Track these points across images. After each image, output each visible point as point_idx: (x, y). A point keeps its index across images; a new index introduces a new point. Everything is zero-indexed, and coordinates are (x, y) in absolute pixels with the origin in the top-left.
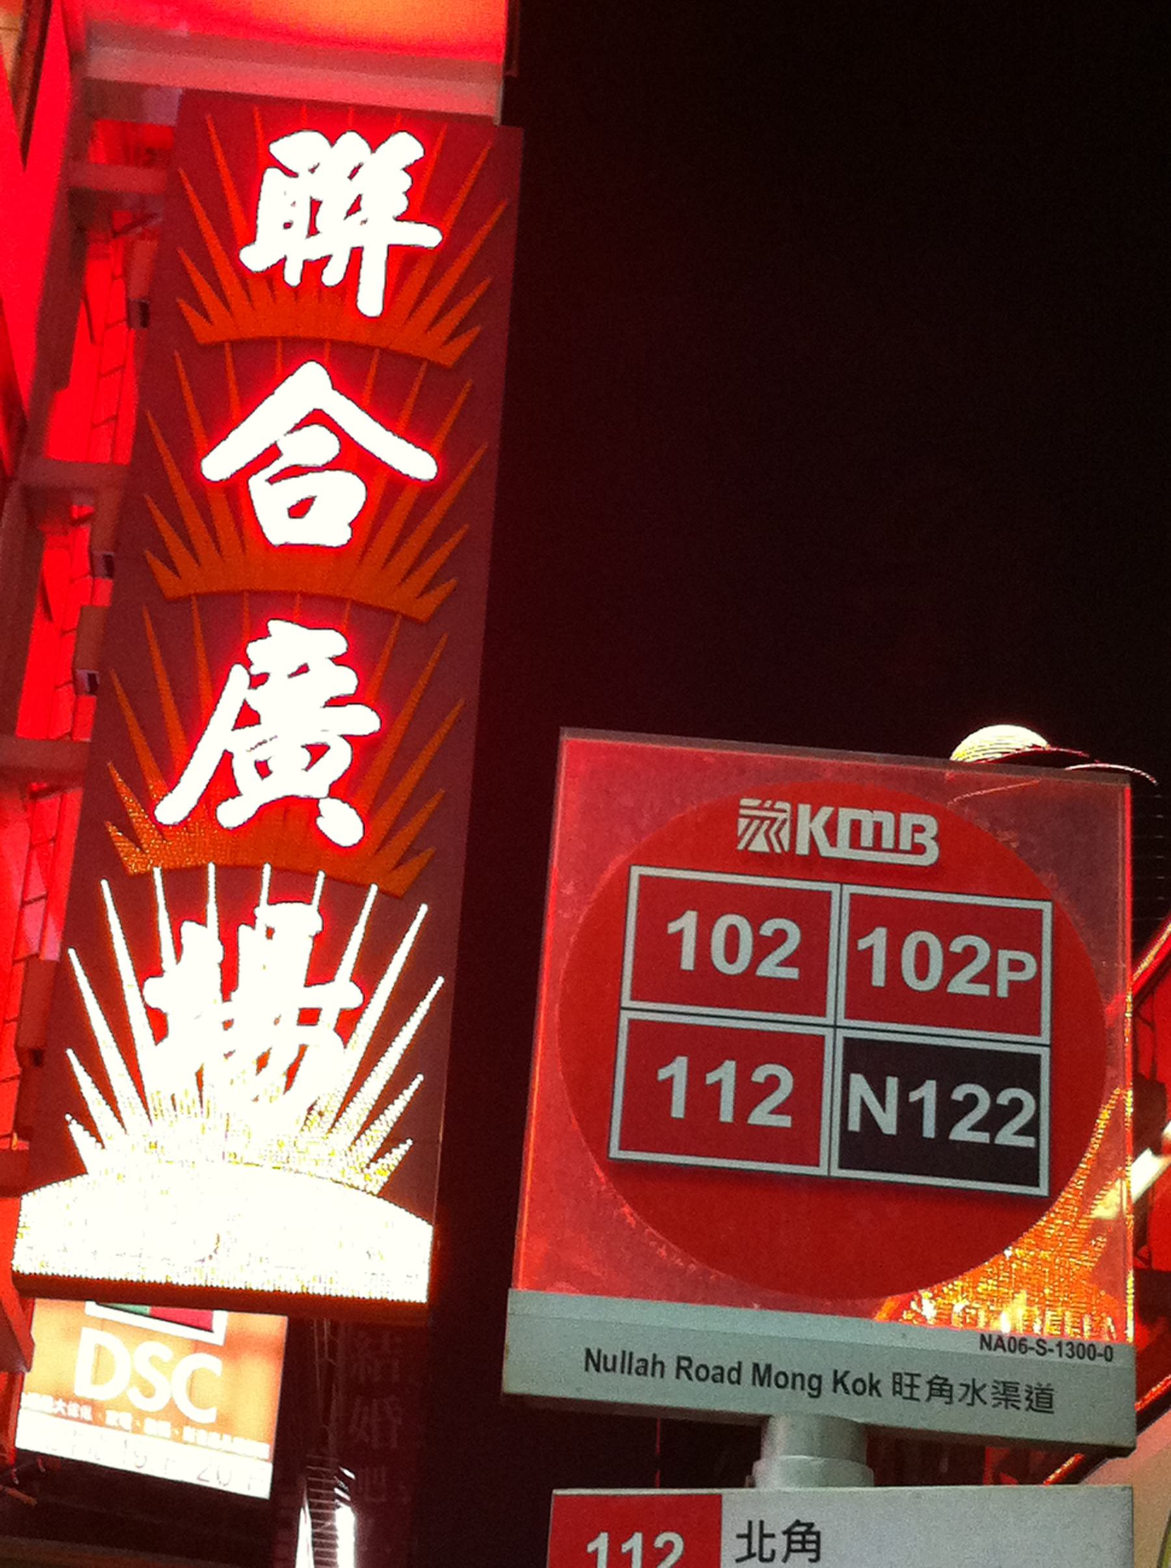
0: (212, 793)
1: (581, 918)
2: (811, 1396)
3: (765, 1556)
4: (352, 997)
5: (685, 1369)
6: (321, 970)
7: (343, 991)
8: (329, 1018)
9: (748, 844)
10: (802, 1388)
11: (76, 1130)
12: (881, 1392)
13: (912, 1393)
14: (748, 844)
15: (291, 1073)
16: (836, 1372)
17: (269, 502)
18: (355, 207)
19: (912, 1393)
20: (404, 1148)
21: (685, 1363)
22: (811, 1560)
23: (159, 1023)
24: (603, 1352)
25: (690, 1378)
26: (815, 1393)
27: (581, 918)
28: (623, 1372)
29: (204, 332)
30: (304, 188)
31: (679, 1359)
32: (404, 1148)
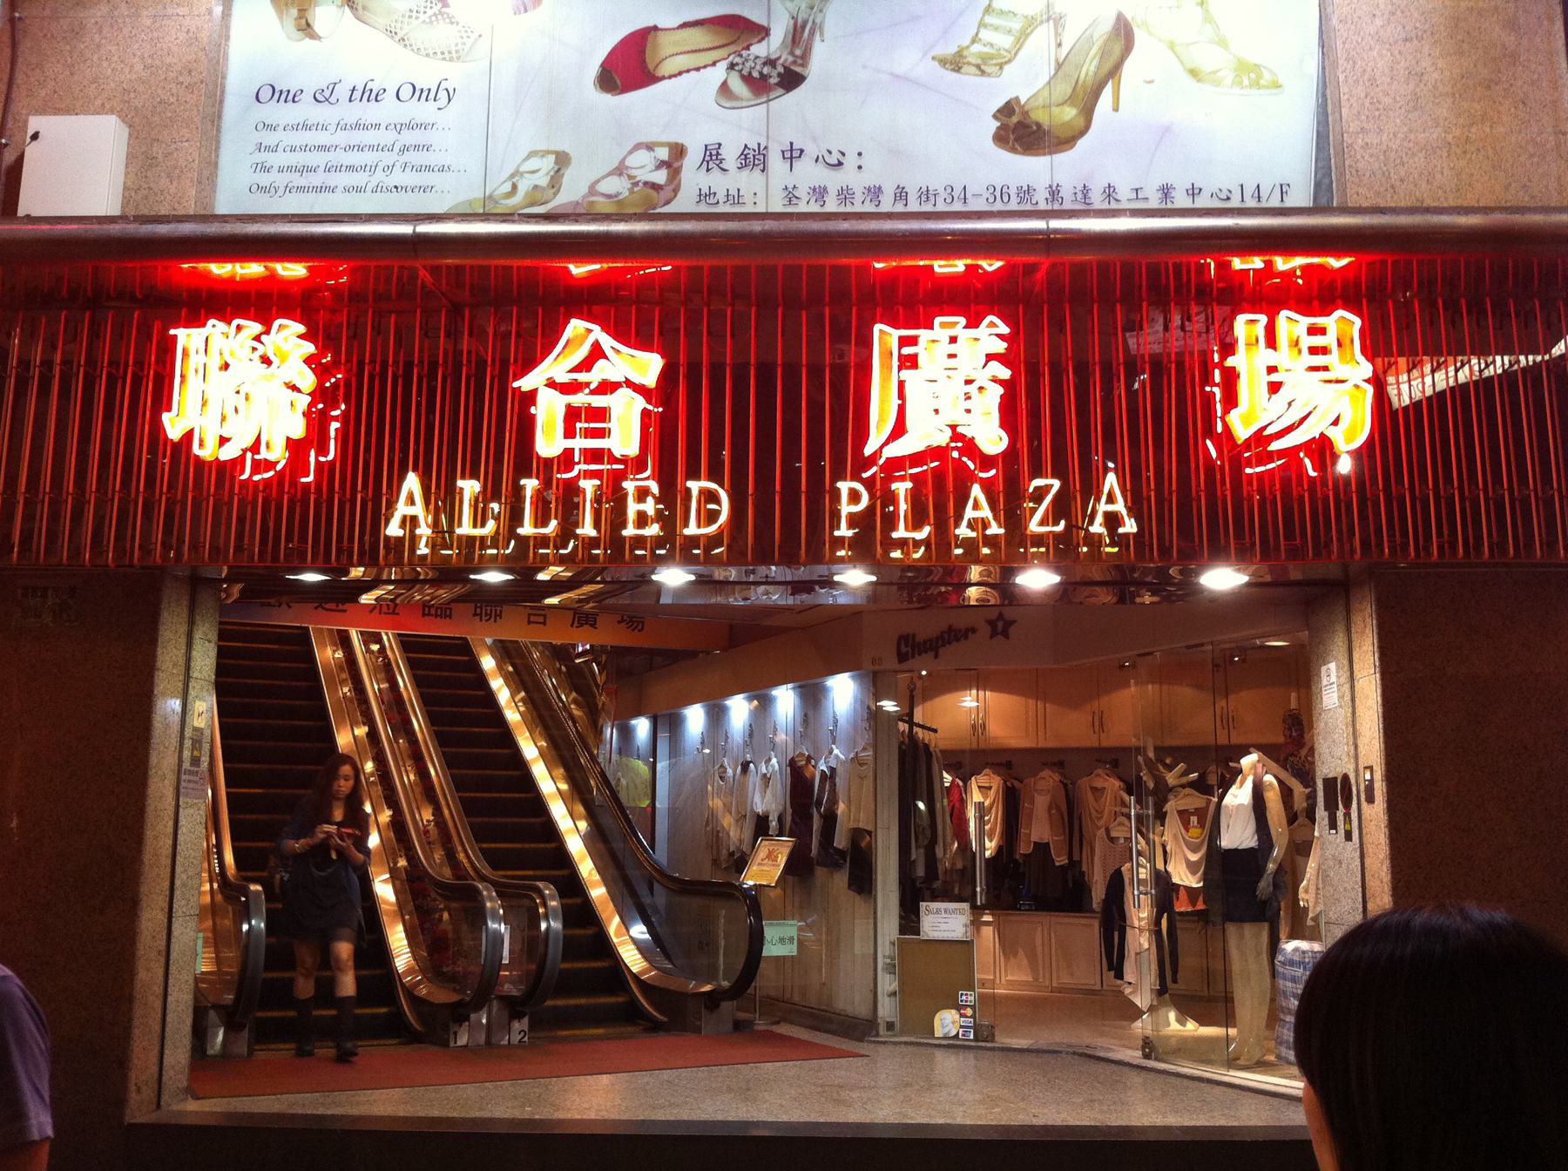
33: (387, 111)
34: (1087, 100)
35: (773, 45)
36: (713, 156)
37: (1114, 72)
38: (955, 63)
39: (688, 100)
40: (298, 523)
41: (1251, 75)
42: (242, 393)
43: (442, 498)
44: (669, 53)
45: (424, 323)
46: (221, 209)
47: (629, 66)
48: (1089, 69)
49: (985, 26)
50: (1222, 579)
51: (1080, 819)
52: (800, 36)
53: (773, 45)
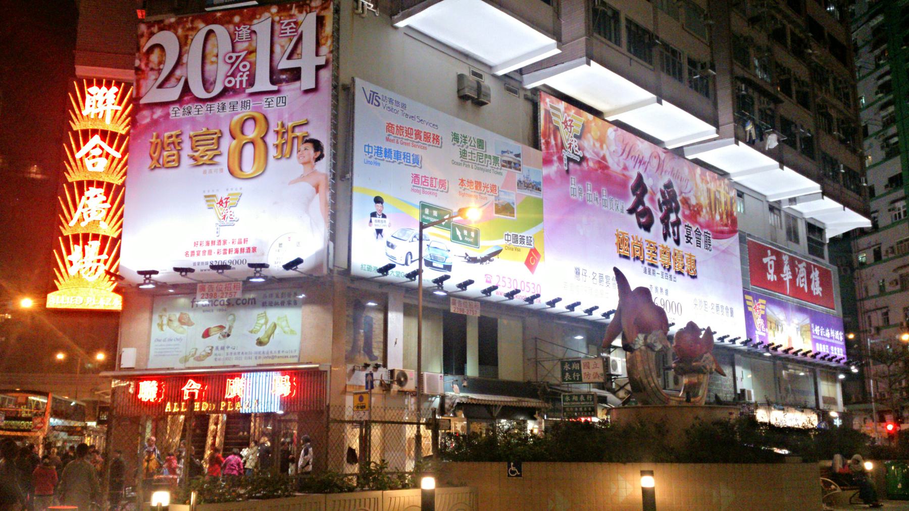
1: (453, 393)
4: (107, 257)
6: (101, 252)
7: (104, 256)
8: (102, 261)
11: (56, 282)
15: (96, 270)
17: (88, 163)
18: (105, 102)
20: (131, 106)
23: (71, 263)
27: (453, 393)
29: (75, 129)
30: (94, 98)
32: (131, 106)
33: (173, 343)
34: (269, 337)
35: (226, 330)
36: (217, 348)
37: (273, 333)
38: (251, 332)
39: (215, 339)
40: (155, 409)
41: (292, 332)
42: (148, 391)
43: (172, 406)
44: (212, 332)
45: (173, 382)
46: (149, 367)
47: (206, 334)
48: (270, 332)
49: (426, 227)
50: (60, 356)
51: (120, 356)
52: (230, 328)
53: (226, 330)
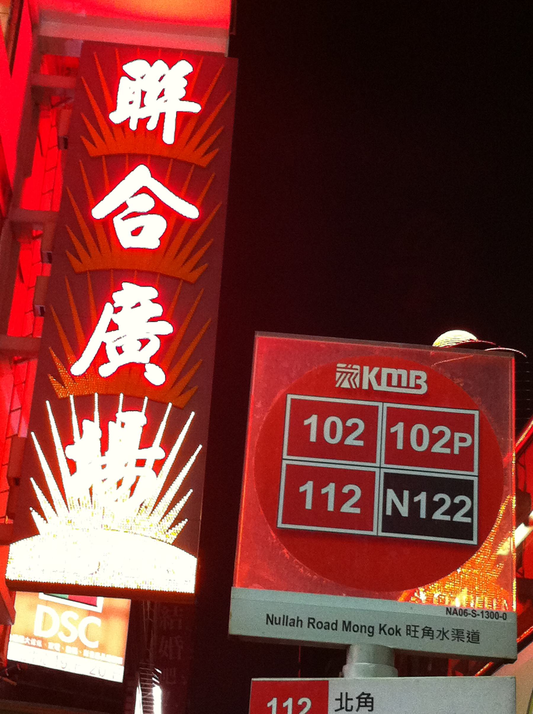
0: (97, 361)
1: (265, 418)
2: (369, 636)
3: (348, 709)
4: (160, 454)
5: (312, 623)
6: (146, 442)
7: (156, 451)
8: (150, 464)
9: (341, 384)
10: (365, 632)
11: (35, 515)
12: (401, 634)
13: (415, 634)
14: (341, 384)
15: (133, 489)
16: (380, 625)
17: (123, 229)
18: (162, 94)
19: (415, 634)
20: (184, 523)
21: (312, 621)
22: (369, 711)
23: (72, 466)
24: (275, 616)
25: (314, 628)
26: (371, 634)
27: (265, 418)
28: (283, 625)
29: (93, 151)
30: (138, 86)
31: (309, 619)
32: (184, 523)
